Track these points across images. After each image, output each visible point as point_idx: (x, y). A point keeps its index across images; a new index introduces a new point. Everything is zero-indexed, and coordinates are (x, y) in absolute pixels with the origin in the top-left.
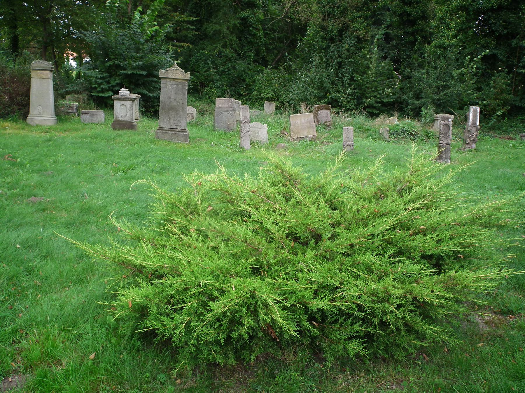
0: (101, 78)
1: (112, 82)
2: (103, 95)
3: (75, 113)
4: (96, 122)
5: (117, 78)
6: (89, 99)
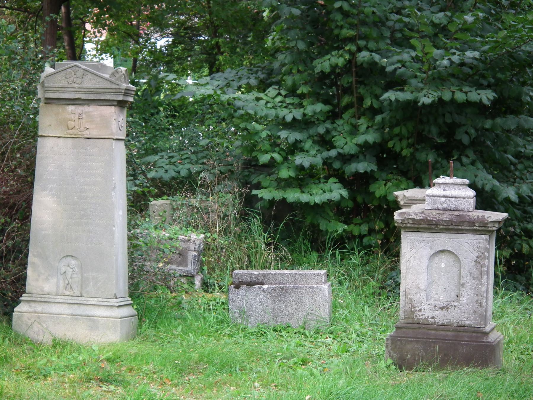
0: (294, 125)
1: (339, 141)
2: (305, 198)
3: (190, 277)
4: (295, 322)
5: (363, 123)
6: (244, 216)
